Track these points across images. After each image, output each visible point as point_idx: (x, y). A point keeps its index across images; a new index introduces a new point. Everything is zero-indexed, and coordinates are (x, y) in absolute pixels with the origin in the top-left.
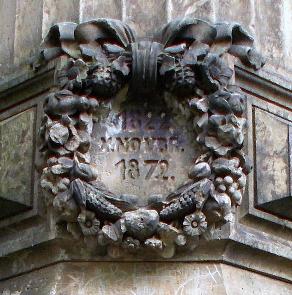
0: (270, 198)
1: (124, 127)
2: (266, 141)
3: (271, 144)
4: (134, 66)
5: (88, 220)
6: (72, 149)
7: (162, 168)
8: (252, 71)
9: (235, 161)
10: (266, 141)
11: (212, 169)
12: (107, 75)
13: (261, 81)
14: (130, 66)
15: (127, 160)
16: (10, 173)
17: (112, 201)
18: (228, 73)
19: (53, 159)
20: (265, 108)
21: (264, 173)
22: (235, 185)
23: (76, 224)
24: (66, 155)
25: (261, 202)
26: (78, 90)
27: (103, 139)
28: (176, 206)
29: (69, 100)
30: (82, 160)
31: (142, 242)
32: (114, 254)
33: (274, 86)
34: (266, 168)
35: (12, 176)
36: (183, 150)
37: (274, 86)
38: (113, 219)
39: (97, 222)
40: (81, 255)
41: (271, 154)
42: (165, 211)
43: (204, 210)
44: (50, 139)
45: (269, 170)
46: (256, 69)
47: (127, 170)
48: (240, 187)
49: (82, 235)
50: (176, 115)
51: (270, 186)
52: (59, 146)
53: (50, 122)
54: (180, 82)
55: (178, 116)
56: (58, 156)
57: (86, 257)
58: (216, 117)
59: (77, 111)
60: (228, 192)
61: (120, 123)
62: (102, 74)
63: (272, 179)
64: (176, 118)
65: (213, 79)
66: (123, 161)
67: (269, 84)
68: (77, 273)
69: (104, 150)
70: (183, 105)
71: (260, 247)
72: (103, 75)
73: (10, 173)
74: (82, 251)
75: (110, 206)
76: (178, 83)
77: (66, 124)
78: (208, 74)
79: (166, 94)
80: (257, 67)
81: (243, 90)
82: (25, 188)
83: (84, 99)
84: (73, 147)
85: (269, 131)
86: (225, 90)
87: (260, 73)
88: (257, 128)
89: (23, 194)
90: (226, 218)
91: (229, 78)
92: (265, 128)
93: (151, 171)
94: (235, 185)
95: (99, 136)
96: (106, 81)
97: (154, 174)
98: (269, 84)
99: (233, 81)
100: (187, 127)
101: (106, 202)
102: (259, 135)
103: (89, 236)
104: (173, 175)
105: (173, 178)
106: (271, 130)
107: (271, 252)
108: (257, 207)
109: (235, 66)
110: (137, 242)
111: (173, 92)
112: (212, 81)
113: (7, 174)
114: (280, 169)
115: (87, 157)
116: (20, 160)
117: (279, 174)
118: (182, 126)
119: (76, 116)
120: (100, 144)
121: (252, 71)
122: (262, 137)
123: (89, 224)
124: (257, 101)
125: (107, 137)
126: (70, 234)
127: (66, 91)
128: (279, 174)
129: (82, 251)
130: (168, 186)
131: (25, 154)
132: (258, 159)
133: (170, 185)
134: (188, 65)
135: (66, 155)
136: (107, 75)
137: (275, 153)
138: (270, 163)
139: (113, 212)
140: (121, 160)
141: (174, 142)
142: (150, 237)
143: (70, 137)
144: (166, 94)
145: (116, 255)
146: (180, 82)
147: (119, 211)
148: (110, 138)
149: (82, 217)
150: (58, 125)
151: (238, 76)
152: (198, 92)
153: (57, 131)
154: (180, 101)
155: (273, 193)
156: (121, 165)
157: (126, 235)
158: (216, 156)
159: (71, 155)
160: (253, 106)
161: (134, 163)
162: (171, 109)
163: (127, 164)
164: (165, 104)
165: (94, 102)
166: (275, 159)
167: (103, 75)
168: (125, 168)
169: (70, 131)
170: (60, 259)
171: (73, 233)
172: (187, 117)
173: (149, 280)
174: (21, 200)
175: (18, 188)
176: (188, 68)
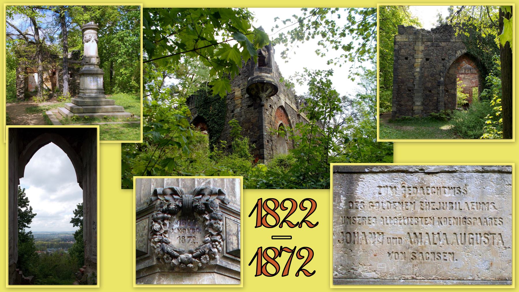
0: (231, 250)
1: (180, 225)
3: (232, 231)
5: (167, 257)
9: (219, 237)
14: (182, 203)
15: (181, 236)
17: (176, 251)
18: (217, 206)
19: (155, 236)
25: (228, 251)
26: (164, 212)
27: (173, 229)
29: (161, 215)
30: (165, 237)
31: (186, 265)
42: (194, 255)
49: (165, 263)
51: (232, 245)
52: (157, 231)
53: (154, 223)
56: (157, 235)
57: (167, 271)
59: (163, 219)
63: (232, 243)
72: (172, 206)
75: (175, 253)
77: (159, 224)
83: (166, 215)
84: (162, 232)
87: (228, 206)
95: (171, 228)
99: (218, 209)
102: (227, 228)
103: (167, 263)
108: (227, 253)
119: (163, 221)
120: (171, 231)
127: (159, 212)
143: (161, 228)
150: (157, 224)
151: (220, 207)
152: (206, 212)
153: (156, 226)
155: (233, 248)
159: (161, 235)
165: (169, 216)
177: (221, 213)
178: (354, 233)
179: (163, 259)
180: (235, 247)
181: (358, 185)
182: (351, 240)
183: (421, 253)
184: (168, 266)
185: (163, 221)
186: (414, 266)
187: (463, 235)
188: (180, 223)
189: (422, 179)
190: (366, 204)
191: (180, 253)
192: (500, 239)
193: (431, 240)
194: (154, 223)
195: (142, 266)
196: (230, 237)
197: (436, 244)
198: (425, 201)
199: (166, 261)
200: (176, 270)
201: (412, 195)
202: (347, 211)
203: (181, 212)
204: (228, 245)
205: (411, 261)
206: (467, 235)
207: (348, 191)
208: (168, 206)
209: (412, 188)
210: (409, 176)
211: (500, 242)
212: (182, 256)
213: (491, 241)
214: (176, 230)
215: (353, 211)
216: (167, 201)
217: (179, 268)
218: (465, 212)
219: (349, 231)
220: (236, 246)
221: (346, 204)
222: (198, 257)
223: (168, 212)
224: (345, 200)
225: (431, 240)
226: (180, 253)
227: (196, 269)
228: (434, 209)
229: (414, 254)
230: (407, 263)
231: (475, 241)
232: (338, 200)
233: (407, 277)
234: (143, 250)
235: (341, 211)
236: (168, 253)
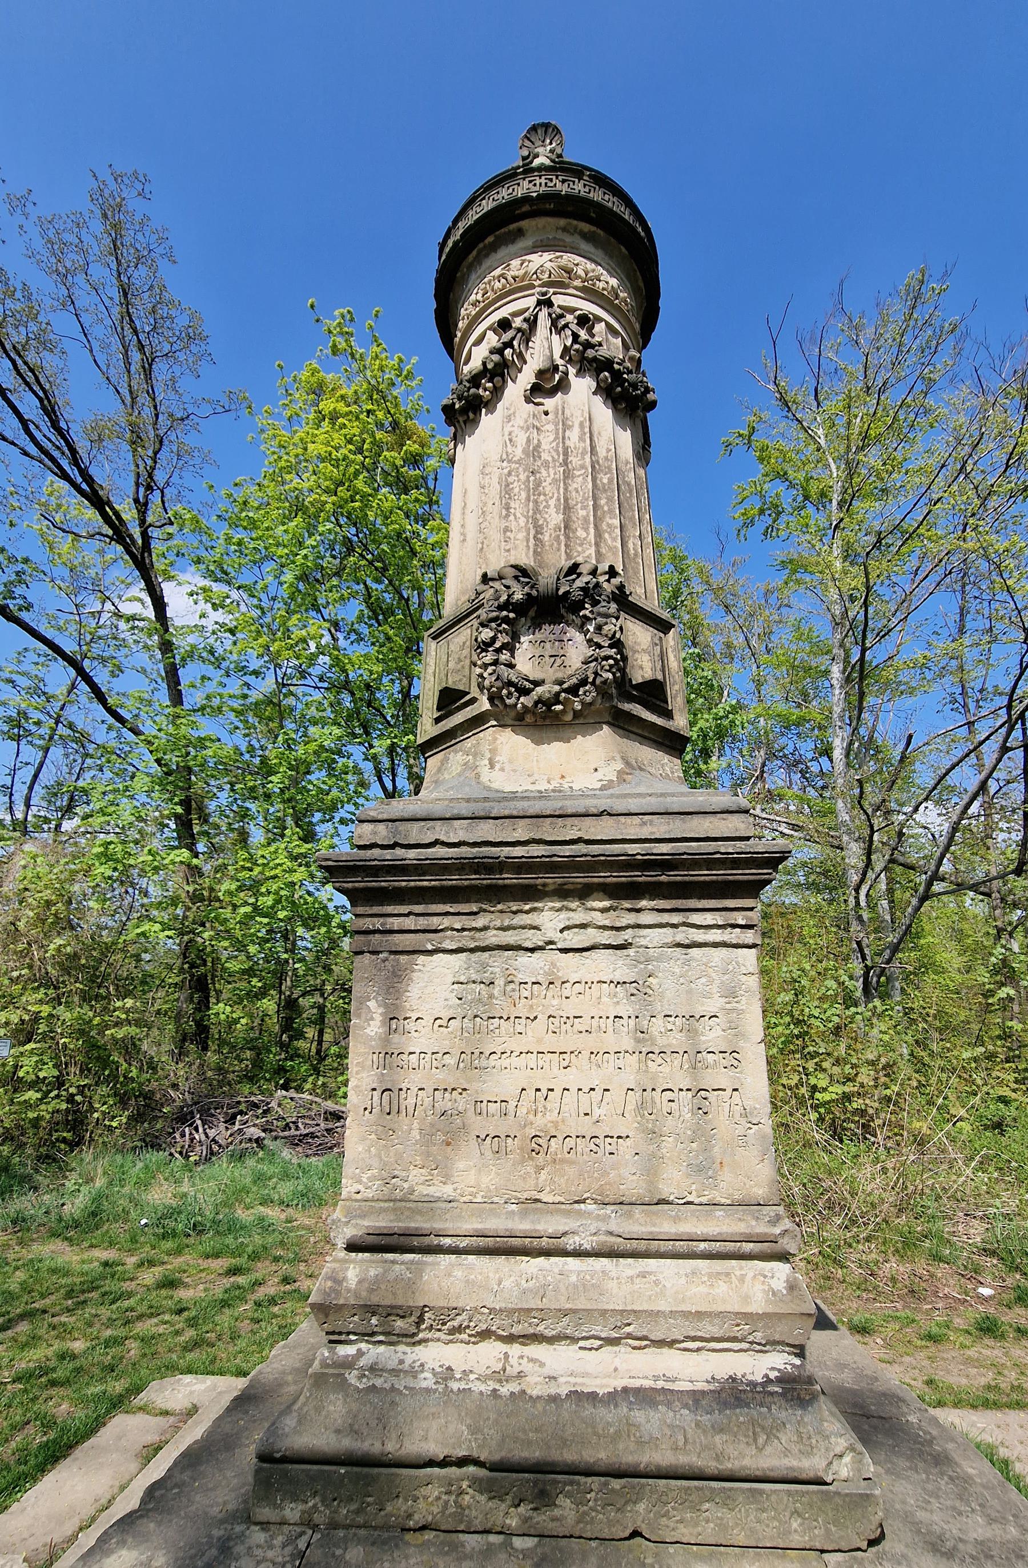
42: (565, 686)
49: (506, 705)
179: (501, 698)
184: (513, 714)
186: (539, 1169)
189: (553, 964)
191: (537, 683)
199: (508, 701)
200: (529, 719)
202: (386, 1040)
205: (532, 1159)
208: (509, 596)
210: (524, 959)
212: (539, 690)
215: (395, 1038)
216: (508, 587)
217: (534, 713)
220: (650, 672)
222: (573, 690)
226: (537, 683)
227: (569, 717)
234: (462, 688)
235: (372, 1039)
236: (510, 683)
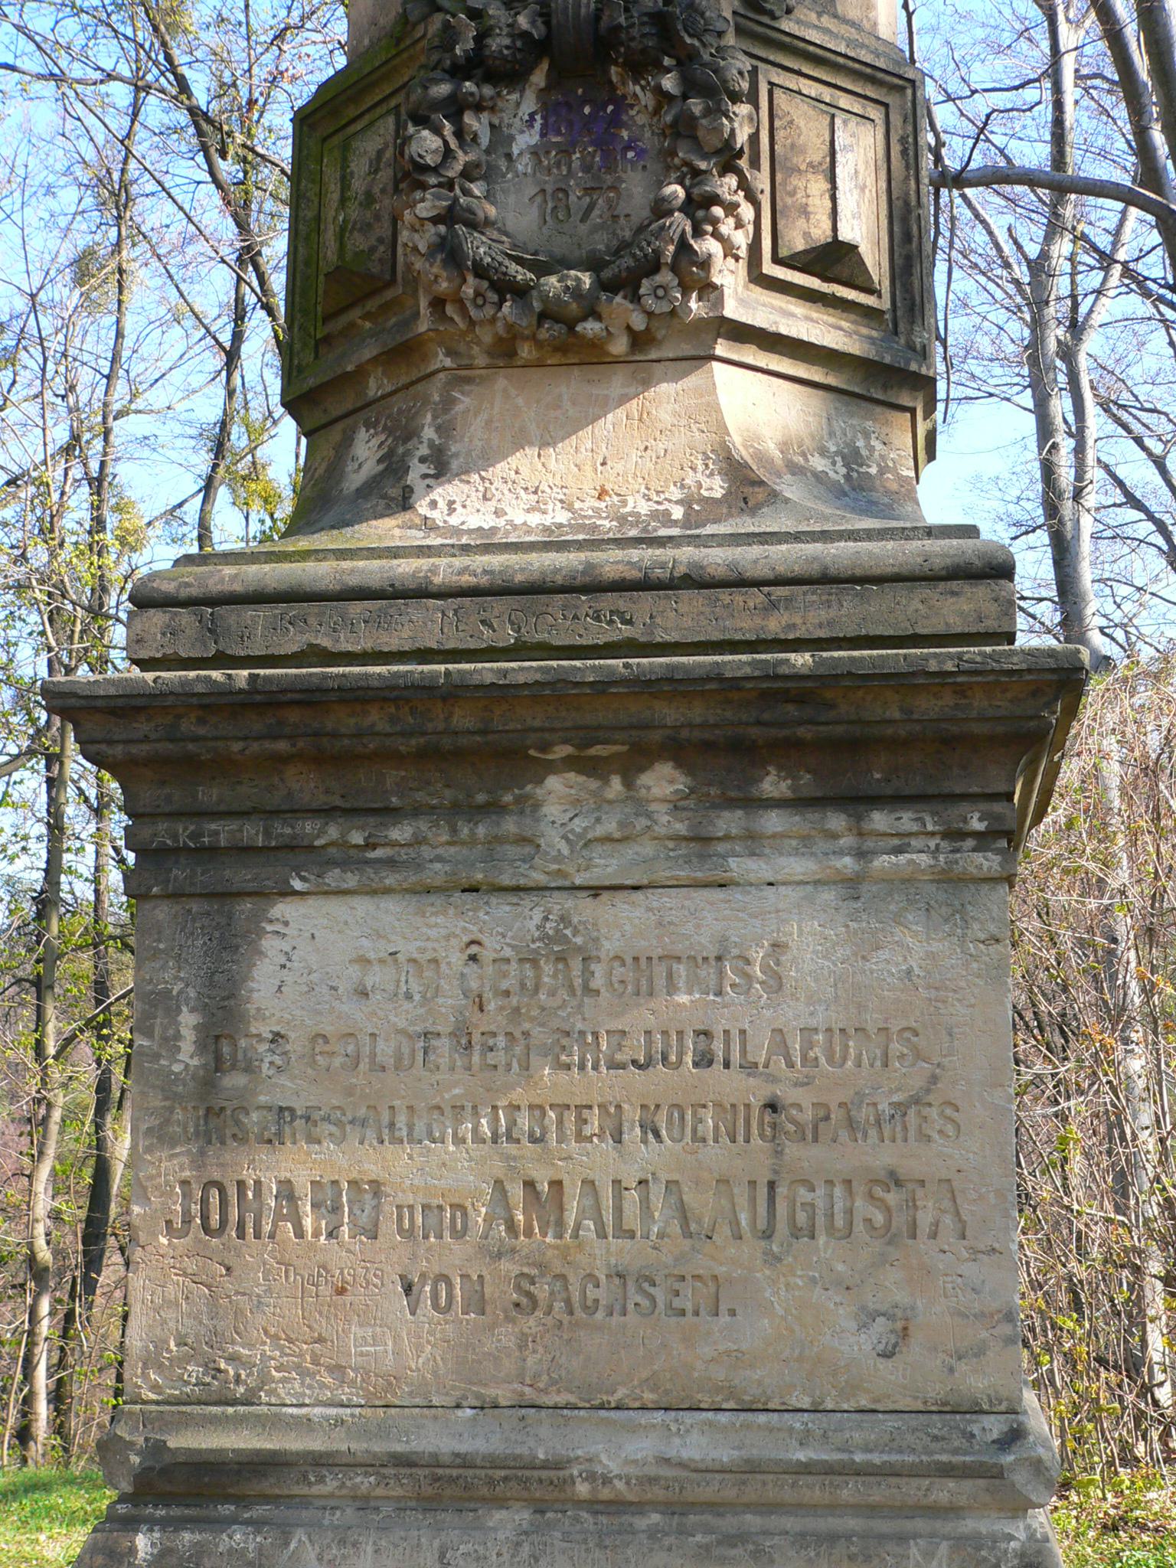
0: (800, 245)
1: (543, 135)
2: (793, 146)
3: (803, 151)
4: (554, 22)
5: (478, 294)
6: (451, 174)
7: (609, 198)
8: (766, 20)
9: (732, 181)
10: (793, 146)
11: (688, 195)
12: (507, 41)
13: (787, 39)
14: (547, 23)
15: (549, 189)
16: (358, 226)
17: (519, 261)
18: (720, 25)
19: (418, 195)
20: (795, 88)
21: (789, 201)
22: (731, 221)
23: (460, 303)
24: (440, 185)
25: (783, 252)
26: (458, 71)
27: (509, 156)
28: (627, 262)
29: (443, 89)
30: (467, 193)
31: (571, 328)
32: (526, 351)
33: (811, 48)
34: (793, 194)
35: (360, 230)
36: (644, 167)
37: (811, 48)
38: (521, 292)
39: (493, 297)
40: (472, 357)
41: (803, 167)
42: (607, 274)
43: (674, 268)
44: (411, 157)
45: (799, 196)
46: (774, 18)
47: (550, 205)
48: (739, 225)
49: (472, 323)
50: (632, 106)
51: (801, 223)
52: (425, 169)
53: (411, 129)
54: (633, 44)
55: (636, 108)
56: (424, 187)
57: (481, 360)
58: (696, 106)
59: (455, 108)
60: (717, 235)
61: (538, 125)
62: (498, 40)
63: (805, 212)
64: (632, 113)
65: (691, 36)
66: (543, 191)
67: (802, 45)
68: (467, 388)
69: (509, 176)
70: (643, 88)
71: (784, 331)
72: (498, 43)
73: (358, 226)
74: (476, 350)
75: (513, 268)
76: (628, 47)
77: (437, 131)
78: (680, 27)
79: (613, 69)
80: (778, 13)
81: (746, 53)
82: (382, 249)
83: (469, 86)
84: (454, 170)
85: (798, 127)
86: (712, 55)
87: (786, 25)
88: (777, 123)
89: (380, 260)
90: (716, 279)
91: (720, 34)
92: (791, 122)
93: (591, 207)
94: (731, 221)
95: (501, 151)
96: (506, 52)
97: (596, 212)
98: (802, 45)
99: (730, 39)
100: (651, 126)
101: (507, 262)
102: (780, 135)
103: (482, 323)
104: (626, 212)
105: (627, 216)
106: (802, 124)
107: (805, 339)
108: (777, 260)
109: (734, 13)
110: (564, 329)
111: (624, 65)
112: (689, 41)
113: (353, 228)
114: (818, 193)
115: (477, 189)
116: (374, 201)
117: (817, 202)
118: (644, 126)
119: (456, 117)
120: (503, 164)
121: (766, 20)
122: (786, 138)
123: (480, 301)
124: (778, 75)
125: (516, 151)
126: (452, 319)
127: (438, 74)
128: (817, 202)
129: (476, 350)
130: (619, 231)
131: (383, 191)
132: (779, 177)
133: (622, 229)
134: (646, 14)
135: (440, 185)
136: (507, 41)
137: (811, 165)
138: (801, 184)
139: (519, 277)
140: (537, 190)
141: (630, 155)
142: (584, 319)
143: (448, 154)
144: (613, 69)
145: (530, 352)
146: (633, 44)
147: (530, 275)
148: (520, 154)
149: (468, 291)
150: (426, 133)
151: (740, 31)
152: (667, 61)
153: (427, 144)
154: (636, 82)
155: (807, 235)
156: (539, 199)
157: (543, 316)
158: (696, 173)
159: (450, 185)
160: (770, 83)
161: (560, 195)
162: (624, 97)
163: (549, 198)
164: (613, 87)
165: (488, 91)
166: (810, 176)
167: (498, 43)
168: (545, 201)
169: (446, 143)
170: (438, 366)
171: (457, 318)
172: (650, 109)
173: (947, 556)
174: (375, 269)
175: (373, 250)
176: (645, 19)
177: (746, 64)
178: (241, 1185)
180: (821, 232)
181: (261, 953)
182: (224, 1222)
183: (562, 1277)
185: (456, 117)
187: (763, 1192)
188: (544, 126)
190: (296, 1044)
192: (947, 1204)
193: (608, 1218)
194: (411, 129)
195: (296, 391)
196: (795, 181)
197: (631, 1235)
198: (579, 1026)
201: (514, 1001)
202: (208, 1082)
203: (545, 66)
204: (781, 224)
205: (509, 1319)
206: (781, 1191)
207: (212, 985)
208: (479, 39)
209: (514, 965)
211: (948, 1220)
213: (900, 1221)
214: (526, 158)
215: (234, 1081)
218: (774, 1079)
219: (216, 1176)
220: (827, 225)
221: (201, 1046)
223: (479, 72)
224: (195, 1028)
225: (608, 1218)
228: (622, 1066)
229: (526, 1285)
230: (492, 1327)
231: (820, 1220)
232: (165, 1028)
233: (491, 1392)
